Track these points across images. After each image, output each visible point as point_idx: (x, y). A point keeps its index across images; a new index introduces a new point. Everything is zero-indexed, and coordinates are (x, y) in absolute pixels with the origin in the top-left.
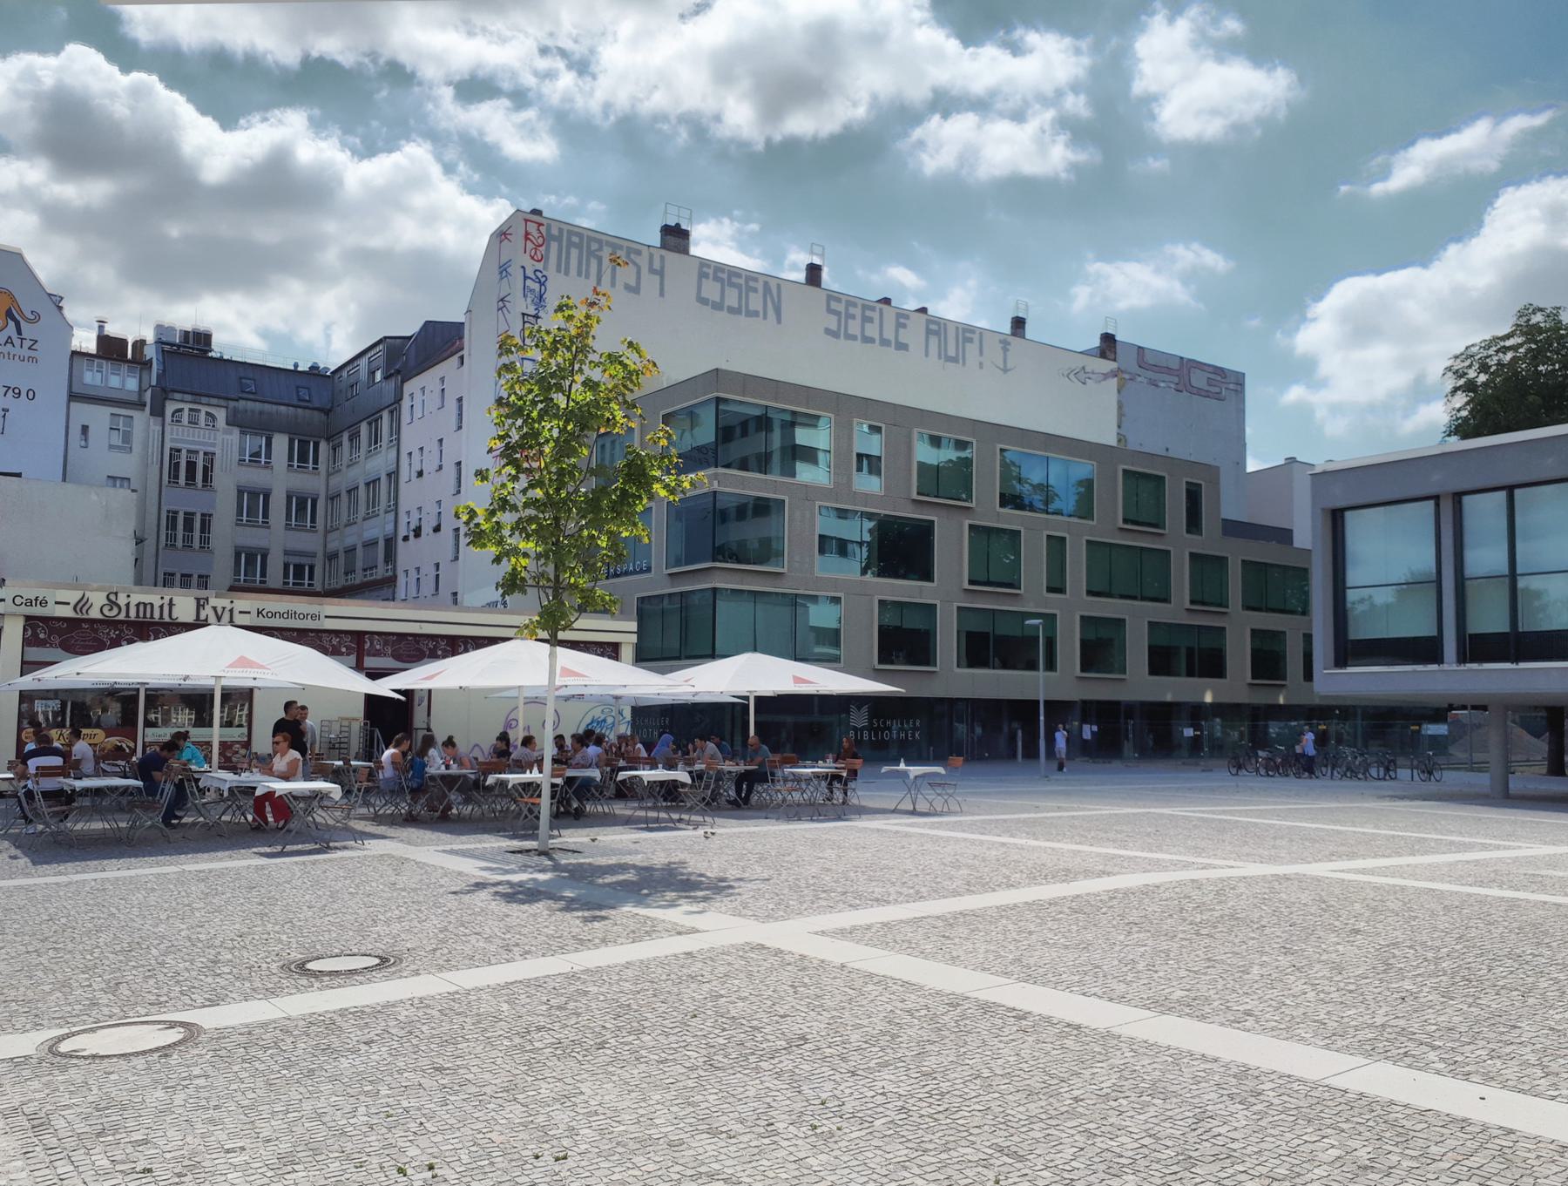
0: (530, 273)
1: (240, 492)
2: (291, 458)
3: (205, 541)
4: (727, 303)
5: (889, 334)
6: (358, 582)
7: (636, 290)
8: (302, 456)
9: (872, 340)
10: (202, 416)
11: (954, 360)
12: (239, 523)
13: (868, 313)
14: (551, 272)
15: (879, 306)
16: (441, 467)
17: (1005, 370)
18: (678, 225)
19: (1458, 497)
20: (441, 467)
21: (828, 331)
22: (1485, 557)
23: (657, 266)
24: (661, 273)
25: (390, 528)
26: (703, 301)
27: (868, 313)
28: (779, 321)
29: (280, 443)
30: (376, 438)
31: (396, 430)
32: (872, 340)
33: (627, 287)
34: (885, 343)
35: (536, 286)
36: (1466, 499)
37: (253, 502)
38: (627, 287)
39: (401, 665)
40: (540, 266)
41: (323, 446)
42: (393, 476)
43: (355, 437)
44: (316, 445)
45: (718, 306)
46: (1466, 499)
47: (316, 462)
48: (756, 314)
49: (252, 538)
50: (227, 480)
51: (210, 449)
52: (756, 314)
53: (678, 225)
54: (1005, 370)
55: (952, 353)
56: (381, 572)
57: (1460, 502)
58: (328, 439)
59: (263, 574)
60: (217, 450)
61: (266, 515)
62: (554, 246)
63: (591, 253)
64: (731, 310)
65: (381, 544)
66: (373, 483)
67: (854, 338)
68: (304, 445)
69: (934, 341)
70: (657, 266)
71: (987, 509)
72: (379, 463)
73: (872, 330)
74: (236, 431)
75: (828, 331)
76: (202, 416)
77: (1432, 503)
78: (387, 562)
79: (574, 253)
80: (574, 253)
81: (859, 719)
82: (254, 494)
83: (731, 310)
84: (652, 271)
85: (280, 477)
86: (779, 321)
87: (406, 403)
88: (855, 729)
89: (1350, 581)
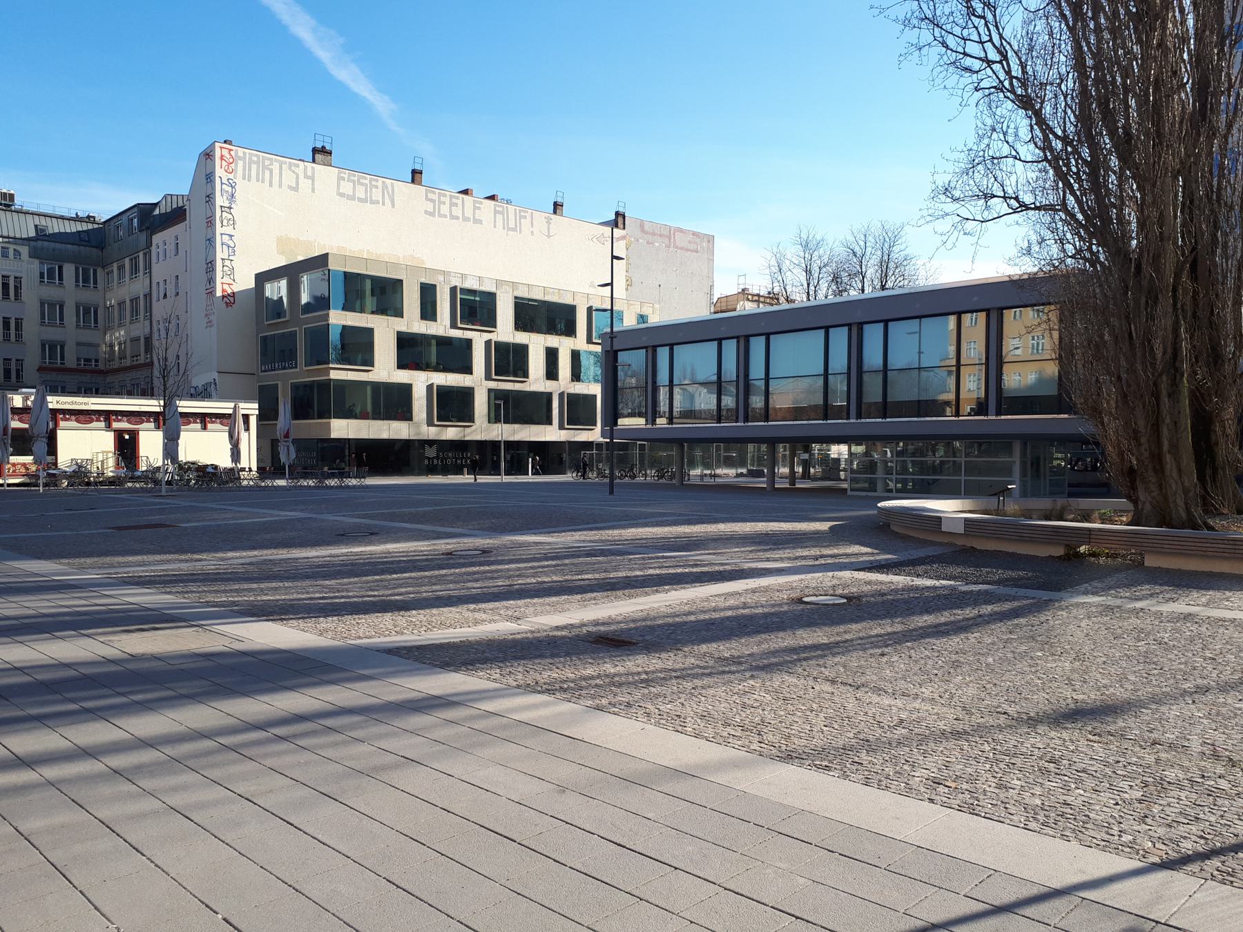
0: (225, 181)
1: (42, 304)
2: (77, 281)
3: (19, 336)
4: (357, 195)
5: (469, 213)
6: (128, 364)
7: (296, 189)
8: (85, 279)
9: (457, 218)
10: (11, 252)
11: (514, 230)
12: (43, 323)
13: (454, 200)
14: (239, 180)
15: (461, 196)
16: (177, 294)
17: (549, 236)
18: (323, 147)
19: (861, 325)
20: (177, 294)
21: (426, 212)
22: (873, 357)
23: (309, 173)
24: (312, 178)
25: (147, 330)
26: (342, 195)
27: (454, 200)
28: (393, 206)
29: (69, 270)
30: (135, 270)
31: (148, 267)
32: (457, 218)
33: (290, 187)
34: (466, 219)
35: (229, 189)
36: (866, 327)
37: (52, 311)
38: (290, 187)
39: (1045, 595)
40: (231, 176)
41: (99, 271)
42: (148, 296)
43: (121, 268)
44: (95, 271)
45: (352, 198)
46: (866, 327)
47: (95, 282)
48: (378, 202)
49: (52, 334)
50: (32, 293)
51: (18, 275)
52: (378, 202)
53: (323, 147)
54: (549, 236)
55: (512, 225)
56: (142, 359)
57: (1002, 314)
58: (103, 267)
59: (62, 358)
60: (24, 275)
61: (62, 319)
62: (240, 163)
63: (265, 167)
64: (360, 200)
65: (142, 340)
66: (135, 300)
67: (445, 216)
68: (86, 272)
69: (499, 217)
70: (309, 173)
71: (505, 330)
72: (138, 287)
73: (457, 211)
74: (36, 262)
75: (426, 212)
76: (11, 252)
77: (846, 328)
78: (146, 352)
79: (254, 167)
80: (254, 167)
81: (431, 452)
82: (52, 305)
83: (360, 200)
84: (306, 177)
85: (69, 291)
86: (393, 206)
87: (154, 248)
88: (429, 459)
89: (751, 377)
